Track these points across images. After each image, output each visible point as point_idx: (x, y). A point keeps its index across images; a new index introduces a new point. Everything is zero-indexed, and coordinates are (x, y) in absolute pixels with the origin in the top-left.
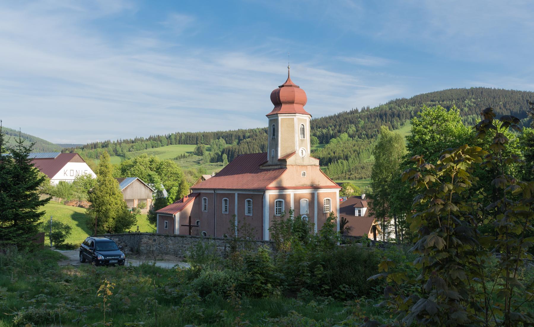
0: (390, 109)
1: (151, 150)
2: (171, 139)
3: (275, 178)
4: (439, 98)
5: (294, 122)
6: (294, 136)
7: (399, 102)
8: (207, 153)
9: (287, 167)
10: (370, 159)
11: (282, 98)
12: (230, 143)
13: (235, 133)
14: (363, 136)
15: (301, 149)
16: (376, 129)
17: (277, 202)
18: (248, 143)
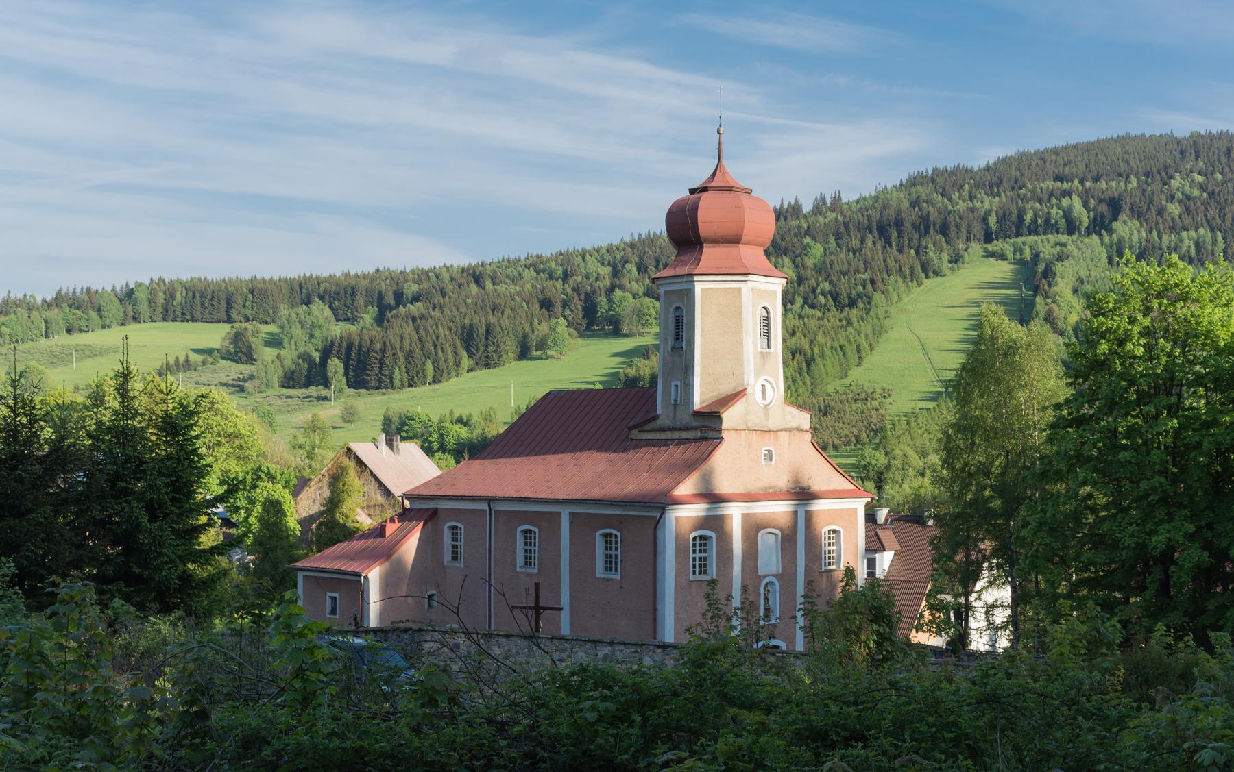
0: (913, 205)
1: (62, 340)
2: (135, 304)
3: (689, 467)
4: (1082, 167)
5: (740, 301)
6: (741, 343)
7: (947, 181)
8: (269, 353)
9: (724, 435)
10: (847, 381)
11: (704, 229)
12: (347, 320)
13: (364, 284)
14: (821, 298)
15: (761, 381)
16: (866, 276)
17: (694, 539)
18: (414, 319)
